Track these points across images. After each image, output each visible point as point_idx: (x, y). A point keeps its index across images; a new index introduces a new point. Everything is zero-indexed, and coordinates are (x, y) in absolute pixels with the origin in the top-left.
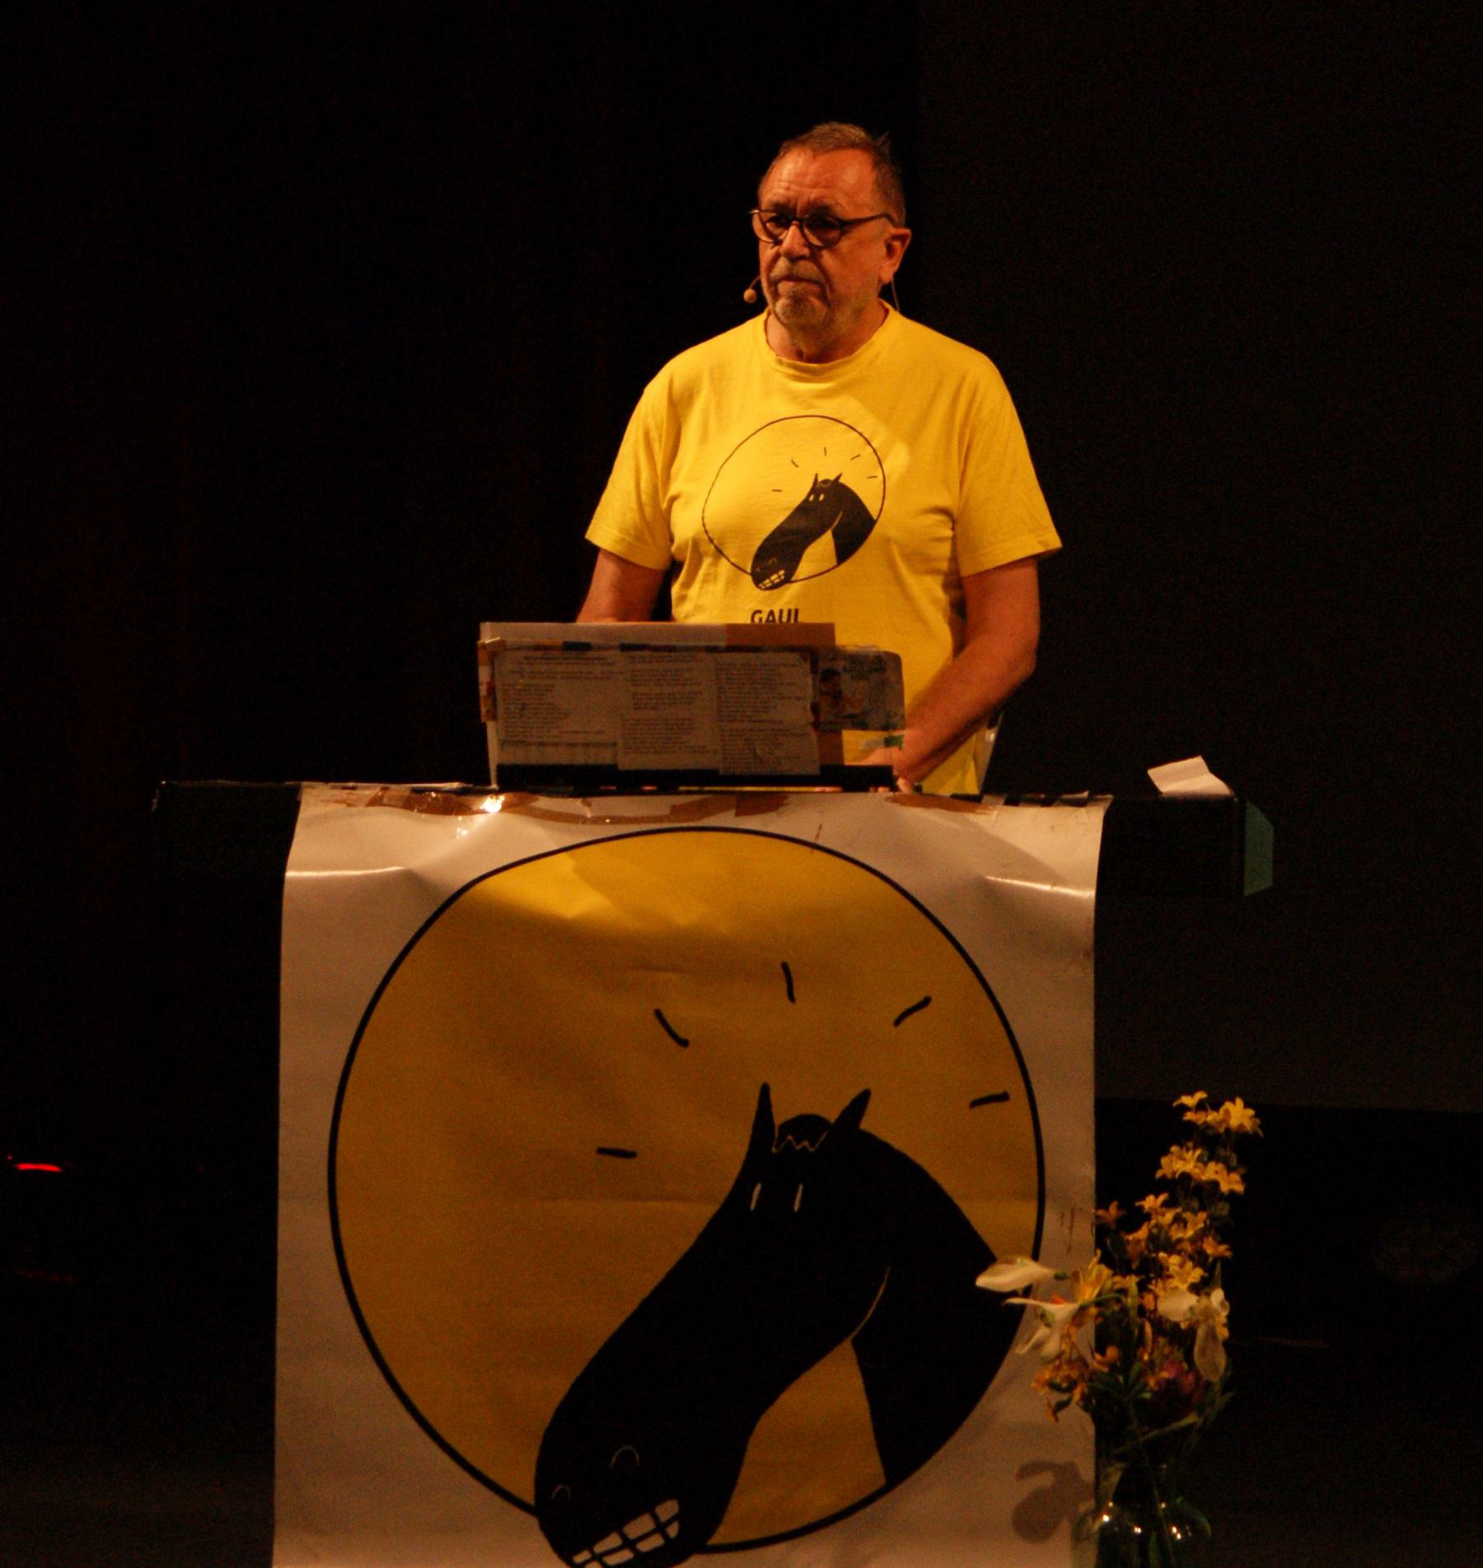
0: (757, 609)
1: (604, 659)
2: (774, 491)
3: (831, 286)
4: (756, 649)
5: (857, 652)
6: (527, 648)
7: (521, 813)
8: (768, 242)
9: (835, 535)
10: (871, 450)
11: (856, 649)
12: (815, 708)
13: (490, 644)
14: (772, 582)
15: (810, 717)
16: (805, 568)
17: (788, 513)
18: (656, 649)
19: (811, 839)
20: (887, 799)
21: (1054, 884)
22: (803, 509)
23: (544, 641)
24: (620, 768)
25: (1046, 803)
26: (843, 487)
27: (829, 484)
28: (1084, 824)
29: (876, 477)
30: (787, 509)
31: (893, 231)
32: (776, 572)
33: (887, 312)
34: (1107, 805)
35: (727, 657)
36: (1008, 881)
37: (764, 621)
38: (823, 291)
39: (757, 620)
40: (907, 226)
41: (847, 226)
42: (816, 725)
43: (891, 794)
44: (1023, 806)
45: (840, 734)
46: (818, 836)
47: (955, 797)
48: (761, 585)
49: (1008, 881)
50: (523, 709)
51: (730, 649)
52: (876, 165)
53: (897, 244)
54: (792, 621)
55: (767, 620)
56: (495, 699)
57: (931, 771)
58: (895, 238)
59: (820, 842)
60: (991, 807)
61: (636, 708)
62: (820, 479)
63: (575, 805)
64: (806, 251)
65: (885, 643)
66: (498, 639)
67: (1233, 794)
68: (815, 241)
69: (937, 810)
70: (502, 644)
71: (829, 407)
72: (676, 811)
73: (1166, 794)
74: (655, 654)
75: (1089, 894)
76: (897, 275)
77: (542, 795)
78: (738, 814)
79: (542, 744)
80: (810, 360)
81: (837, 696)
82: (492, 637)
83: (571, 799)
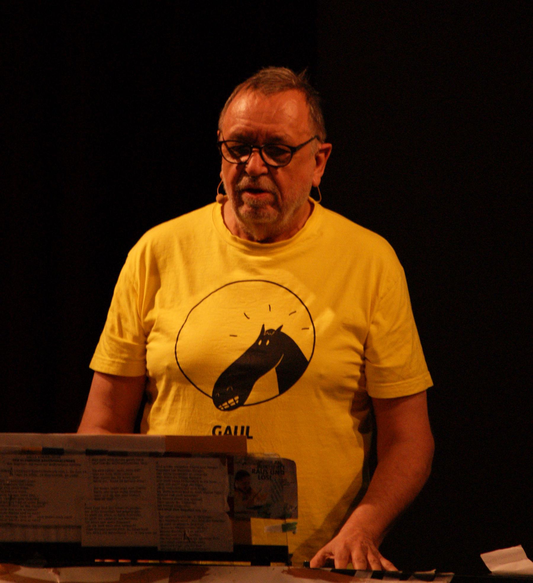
0: (216, 424)
1: (74, 461)
2: (231, 336)
4: (188, 455)
6: (15, 452)
8: (232, 163)
9: (277, 371)
10: (304, 308)
12: (231, 501)
14: (229, 405)
15: (227, 507)
16: (253, 397)
17: (241, 353)
18: (113, 454)
22: (253, 350)
23: (27, 446)
24: (84, 545)
26: (284, 335)
27: (274, 333)
29: (308, 329)
31: (320, 146)
32: (233, 397)
33: (312, 206)
35: (169, 461)
37: (223, 433)
38: (276, 198)
39: (217, 433)
40: (326, 141)
41: (294, 150)
42: (231, 513)
43: (286, 568)
44: (386, 580)
45: (249, 520)
48: (220, 407)
50: (11, 498)
51: (168, 454)
52: (308, 99)
53: (322, 155)
55: (226, 433)
58: (321, 151)
62: (266, 329)
64: (265, 170)
68: (272, 163)
71: (268, 274)
74: (111, 457)
76: (323, 178)
77: (23, 565)
79: (24, 526)
81: (247, 491)
83: (45, 569)
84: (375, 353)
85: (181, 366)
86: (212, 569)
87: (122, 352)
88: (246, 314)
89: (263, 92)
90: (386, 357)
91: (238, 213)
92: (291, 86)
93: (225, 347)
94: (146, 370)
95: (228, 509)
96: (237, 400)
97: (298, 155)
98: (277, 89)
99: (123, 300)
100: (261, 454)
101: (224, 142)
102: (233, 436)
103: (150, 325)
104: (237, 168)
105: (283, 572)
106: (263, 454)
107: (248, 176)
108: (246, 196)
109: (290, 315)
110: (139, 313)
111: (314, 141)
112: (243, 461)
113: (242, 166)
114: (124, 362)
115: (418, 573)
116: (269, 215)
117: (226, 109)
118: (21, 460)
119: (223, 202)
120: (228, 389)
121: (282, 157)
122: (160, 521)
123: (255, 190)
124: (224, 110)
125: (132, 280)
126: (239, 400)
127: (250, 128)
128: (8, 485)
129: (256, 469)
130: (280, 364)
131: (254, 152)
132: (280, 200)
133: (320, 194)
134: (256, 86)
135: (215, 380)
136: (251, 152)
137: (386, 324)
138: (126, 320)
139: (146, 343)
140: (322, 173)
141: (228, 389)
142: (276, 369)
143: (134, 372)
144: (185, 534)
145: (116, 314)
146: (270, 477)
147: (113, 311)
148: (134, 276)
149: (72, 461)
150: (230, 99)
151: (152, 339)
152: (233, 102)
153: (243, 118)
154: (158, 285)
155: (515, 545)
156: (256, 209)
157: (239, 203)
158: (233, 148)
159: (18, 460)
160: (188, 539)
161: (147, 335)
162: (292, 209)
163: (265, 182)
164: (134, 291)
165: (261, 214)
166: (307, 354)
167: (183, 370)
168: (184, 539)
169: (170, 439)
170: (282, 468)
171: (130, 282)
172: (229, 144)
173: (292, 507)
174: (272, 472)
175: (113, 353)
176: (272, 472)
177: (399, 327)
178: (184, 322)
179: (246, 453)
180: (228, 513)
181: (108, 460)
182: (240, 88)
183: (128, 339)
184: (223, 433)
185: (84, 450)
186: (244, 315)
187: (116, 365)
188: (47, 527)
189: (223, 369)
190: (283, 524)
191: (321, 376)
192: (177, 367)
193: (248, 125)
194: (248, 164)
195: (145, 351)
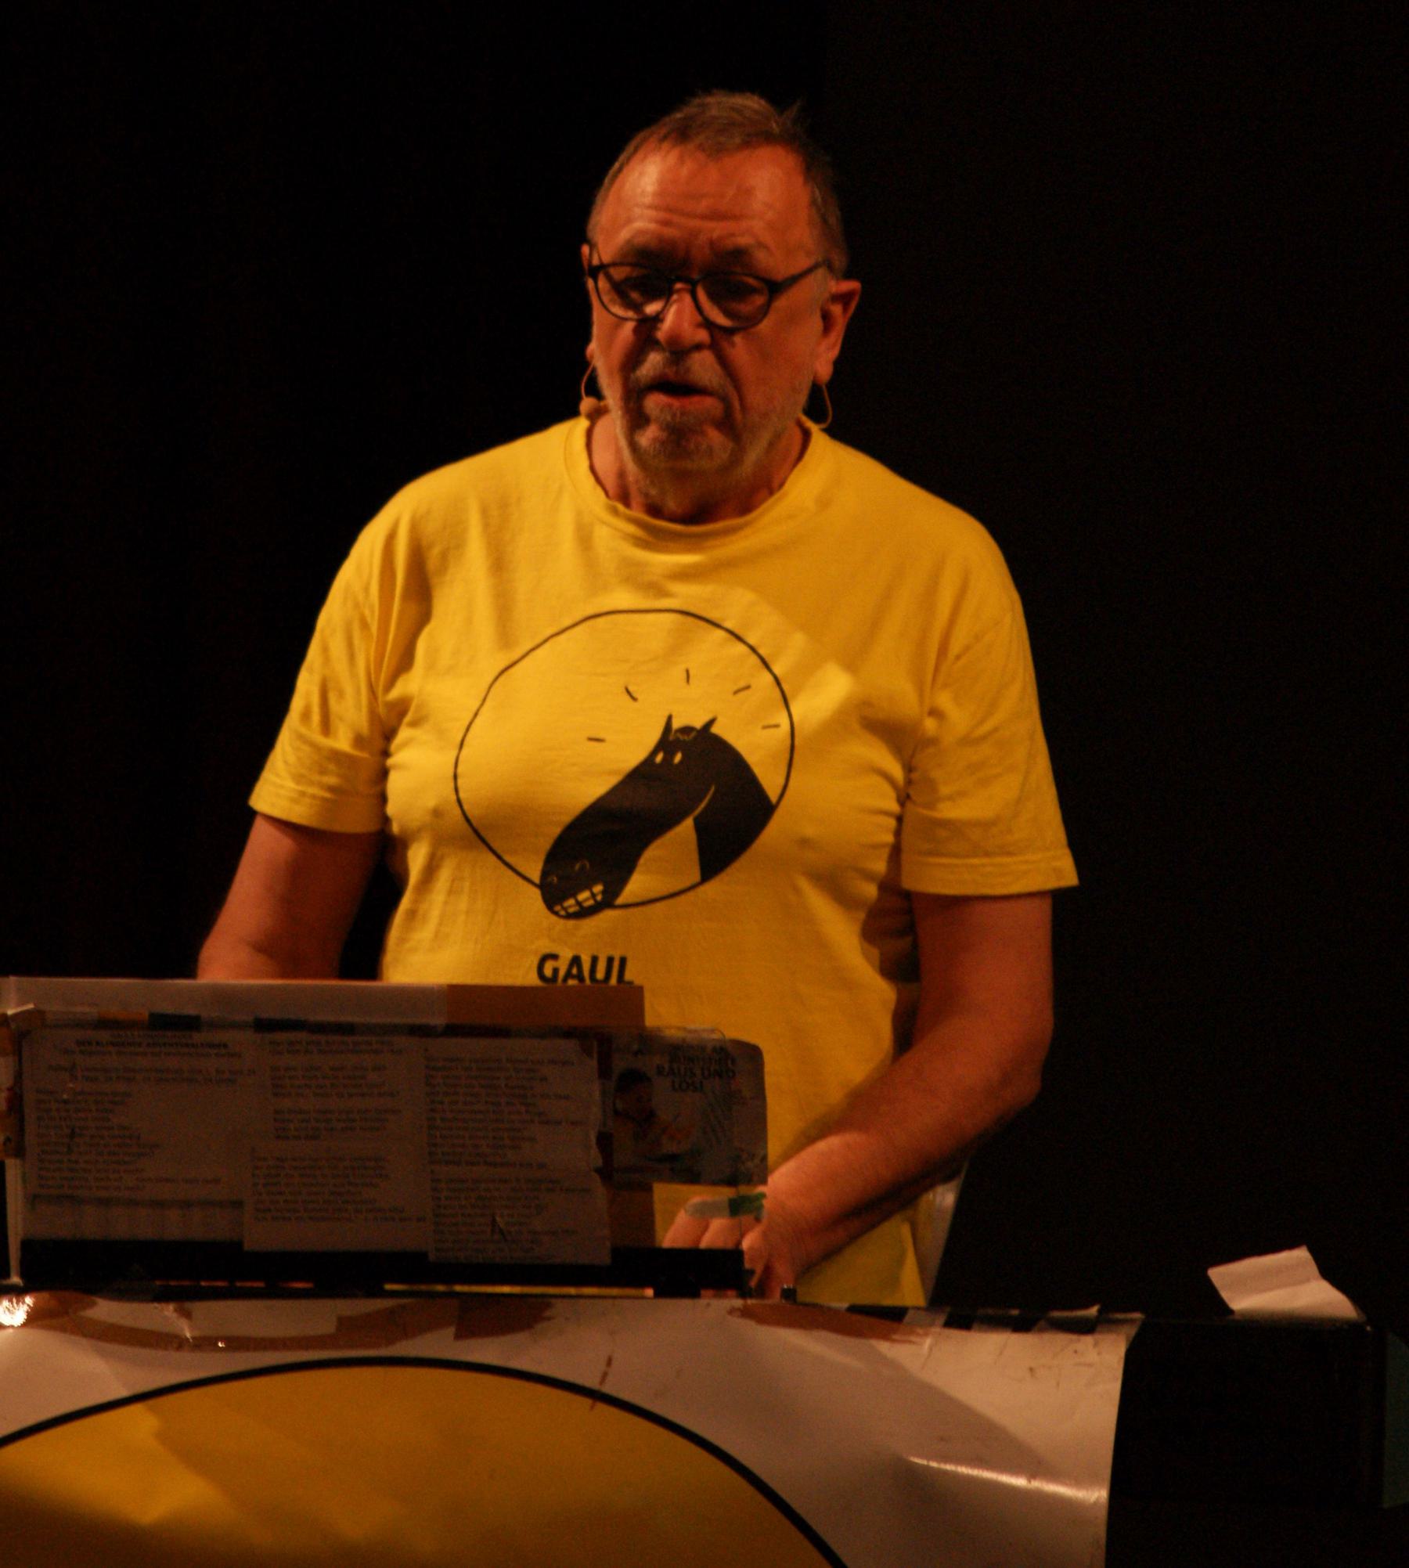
0: (547, 951)
1: (225, 1046)
2: (591, 739)
3: (742, 399)
5: (684, 1040)
6: (80, 1024)
7: (63, 1329)
8: (626, 319)
9: (699, 827)
11: (680, 1034)
12: (605, 1141)
13: (16, 1015)
14: (579, 903)
16: (637, 885)
17: (614, 780)
19: (591, 1382)
20: (732, 1311)
21: (1032, 1476)
22: (642, 774)
25: (1022, 1325)
27: (693, 734)
28: (1090, 1365)
29: (777, 726)
30: (611, 773)
32: (589, 887)
34: (1132, 1330)
36: (949, 1467)
37: (562, 973)
40: (848, 275)
41: (775, 288)
42: (606, 1173)
43: (738, 1303)
44: (980, 1330)
45: (649, 1189)
46: (605, 1375)
47: (854, 1309)
48: (558, 908)
49: (949, 1467)
50: (72, 1135)
51: (452, 1030)
52: (809, 169)
54: (613, 981)
55: (568, 975)
56: (22, 1119)
57: (853, 1239)
58: (837, 298)
59: (607, 1389)
60: (920, 1331)
61: (278, 1137)
62: (676, 724)
63: (165, 1316)
64: (703, 335)
65: (736, 1027)
66: (31, 1006)
67: (1363, 1318)
68: (721, 320)
69: (824, 1334)
70: (37, 1015)
71: (686, 594)
72: (348, 1328)
73: (1243, 1313)
74: (314, 1037)
75: (1097, 1495)
76: (838, 364)
78: (459, 1336)
79: (104, 1202)
80: (673, 519)
81: (645, 1119)
82: (18, 1005)
84: (931, 785)
85: (466, 807)
86: (559, 1305)
87: (323, 772)
88: (631, 689)
89: (701, 147)
90: (950, 798)
91: (634, 446)
92: (769, 138)
93: (574, 765)
94: (386, 820)
95: (599, 1162)
96: (598, 894)
97: (782, 303)
98: (738, 140)
99: (337, 647)
100: (679, 1028)
101: (602, 267)
102: (589, 986)
103: (400, 709)
104: (636, 331)
105: (732, 1311)
106: (685, 1029)
107: (663, 350)
108: (654, 403)
109: (736, 692)
110: (373, 679)
111: (821, 273)
112: (635, 1047)
113: (647, 327)
114: (327, 795)
115: (1056, 1314)
116: (710, 449)
117: (609, 189)
118: (98, 1043)
119: (595, 416)
120: (577, 867)
121: (745, 308)
122: (435, 1189)
123: (675, 386)
124: (602, 192)
125: (361, 598)
126: (604, 892)
127: (670, 232)
128: (66, 1102)
129: (666, 1066)
130: (706, 808)
131: (678, 291)
132: (738, 416)
133: (829, 403)
134: (682, 134)
135: (546, 844)
136: (671, 294)
137: (959, 718)
138: (341, 694)
139: (386, 754)
140: (836, 352)
141: (577, 867)
142: (697, 821)
143: (356, 822)
144: (494, 1220)
145: (317, 679)
146: (702, 1086)
147: (311, 671)
148: (367, 589)
149: (219, 1046)
150: (617, 165)
151: (405, 744)
152: (625, 171)
153: (650, 207)
154: (424, 617)
155: (1291, 1246)
156: (678, 437)
157: (637, 419)
158: (627, 279)
159: (90, 1043)
160: (503, 1234)
161: (389, 735)
162: (765, 437)
163: (703, 367)
164: (364, 625)
165: (692, 446)
166: (771, 783)
167: (470, 817)
168: (493, 1231)
169: (457, 994)
170: (729, 1062)
171: (357, 605)
172: (619, 274)
173: (753, 1156)
174: (706, 1073)
175: (303, 771)
176: (706, 1073)
177: (996, 730)
178: (477, 704)
179: (644, 1028)
180: (598, 1171)
181: (307, 1044)
182: (645, 140)
183: (342, 742)
184: (562, 973)
185: (250, 1019)
186: (624, 691)
187: (307, 800)
188: (158, 1204)
189: (567, 819)
190: (731, 1196)
191: (804, 842)
192: (457, 811)
193: (666, 223)
194: (662, 320)
195: (384, 774)
